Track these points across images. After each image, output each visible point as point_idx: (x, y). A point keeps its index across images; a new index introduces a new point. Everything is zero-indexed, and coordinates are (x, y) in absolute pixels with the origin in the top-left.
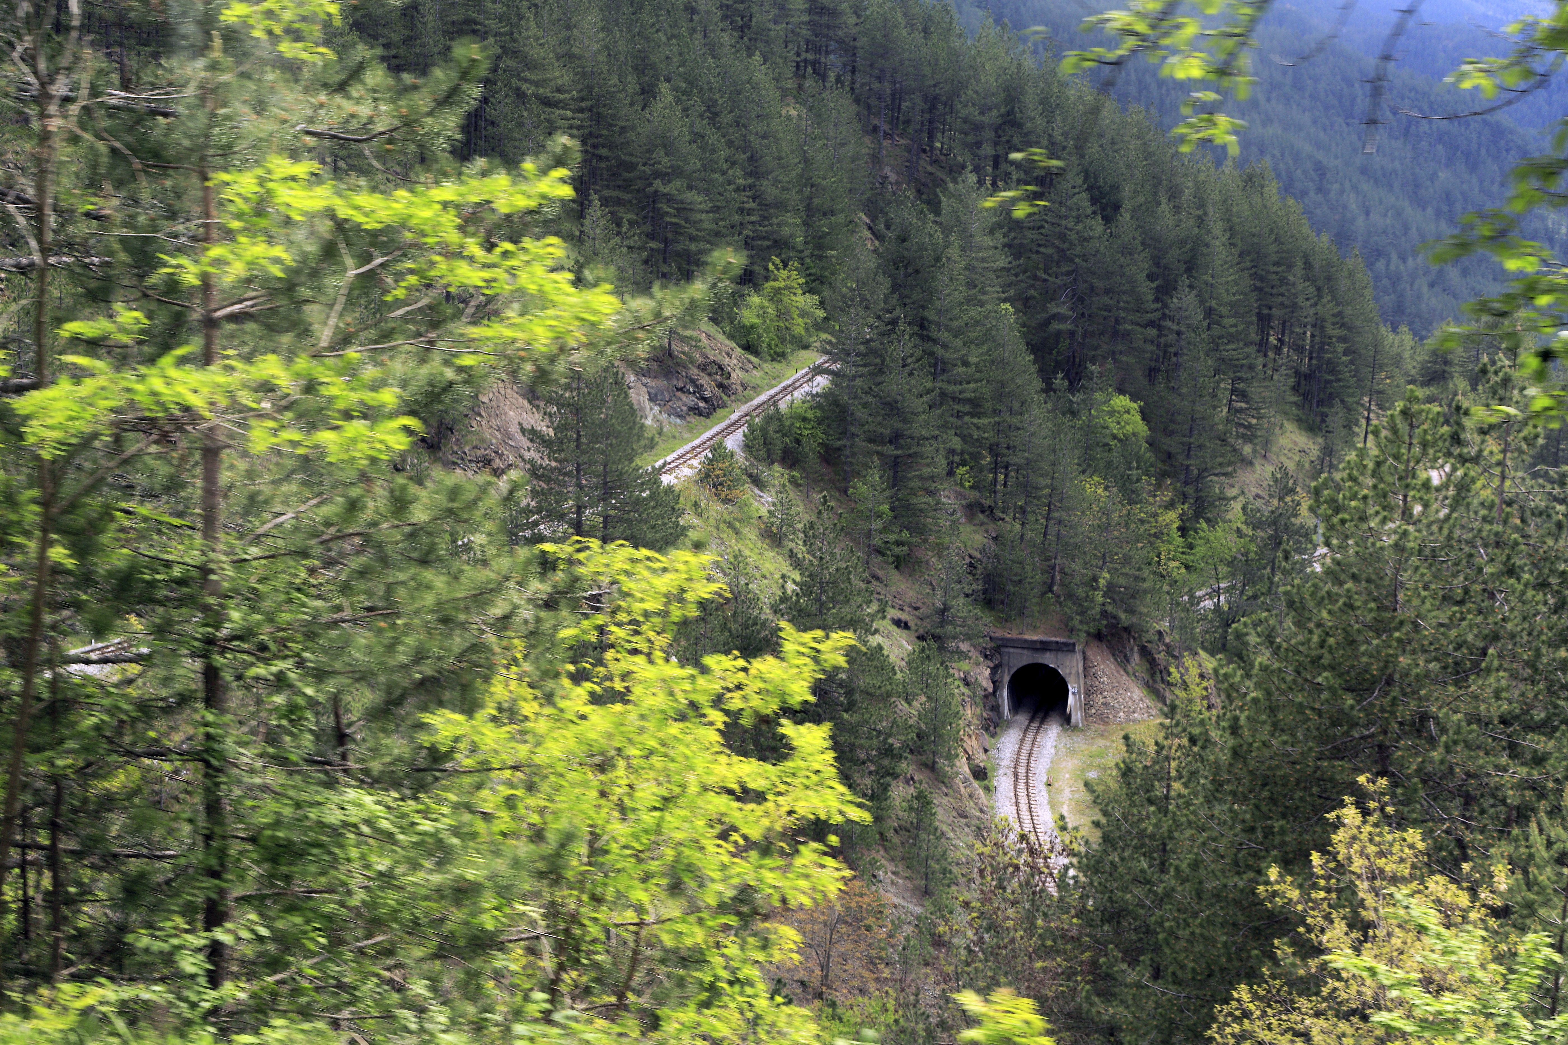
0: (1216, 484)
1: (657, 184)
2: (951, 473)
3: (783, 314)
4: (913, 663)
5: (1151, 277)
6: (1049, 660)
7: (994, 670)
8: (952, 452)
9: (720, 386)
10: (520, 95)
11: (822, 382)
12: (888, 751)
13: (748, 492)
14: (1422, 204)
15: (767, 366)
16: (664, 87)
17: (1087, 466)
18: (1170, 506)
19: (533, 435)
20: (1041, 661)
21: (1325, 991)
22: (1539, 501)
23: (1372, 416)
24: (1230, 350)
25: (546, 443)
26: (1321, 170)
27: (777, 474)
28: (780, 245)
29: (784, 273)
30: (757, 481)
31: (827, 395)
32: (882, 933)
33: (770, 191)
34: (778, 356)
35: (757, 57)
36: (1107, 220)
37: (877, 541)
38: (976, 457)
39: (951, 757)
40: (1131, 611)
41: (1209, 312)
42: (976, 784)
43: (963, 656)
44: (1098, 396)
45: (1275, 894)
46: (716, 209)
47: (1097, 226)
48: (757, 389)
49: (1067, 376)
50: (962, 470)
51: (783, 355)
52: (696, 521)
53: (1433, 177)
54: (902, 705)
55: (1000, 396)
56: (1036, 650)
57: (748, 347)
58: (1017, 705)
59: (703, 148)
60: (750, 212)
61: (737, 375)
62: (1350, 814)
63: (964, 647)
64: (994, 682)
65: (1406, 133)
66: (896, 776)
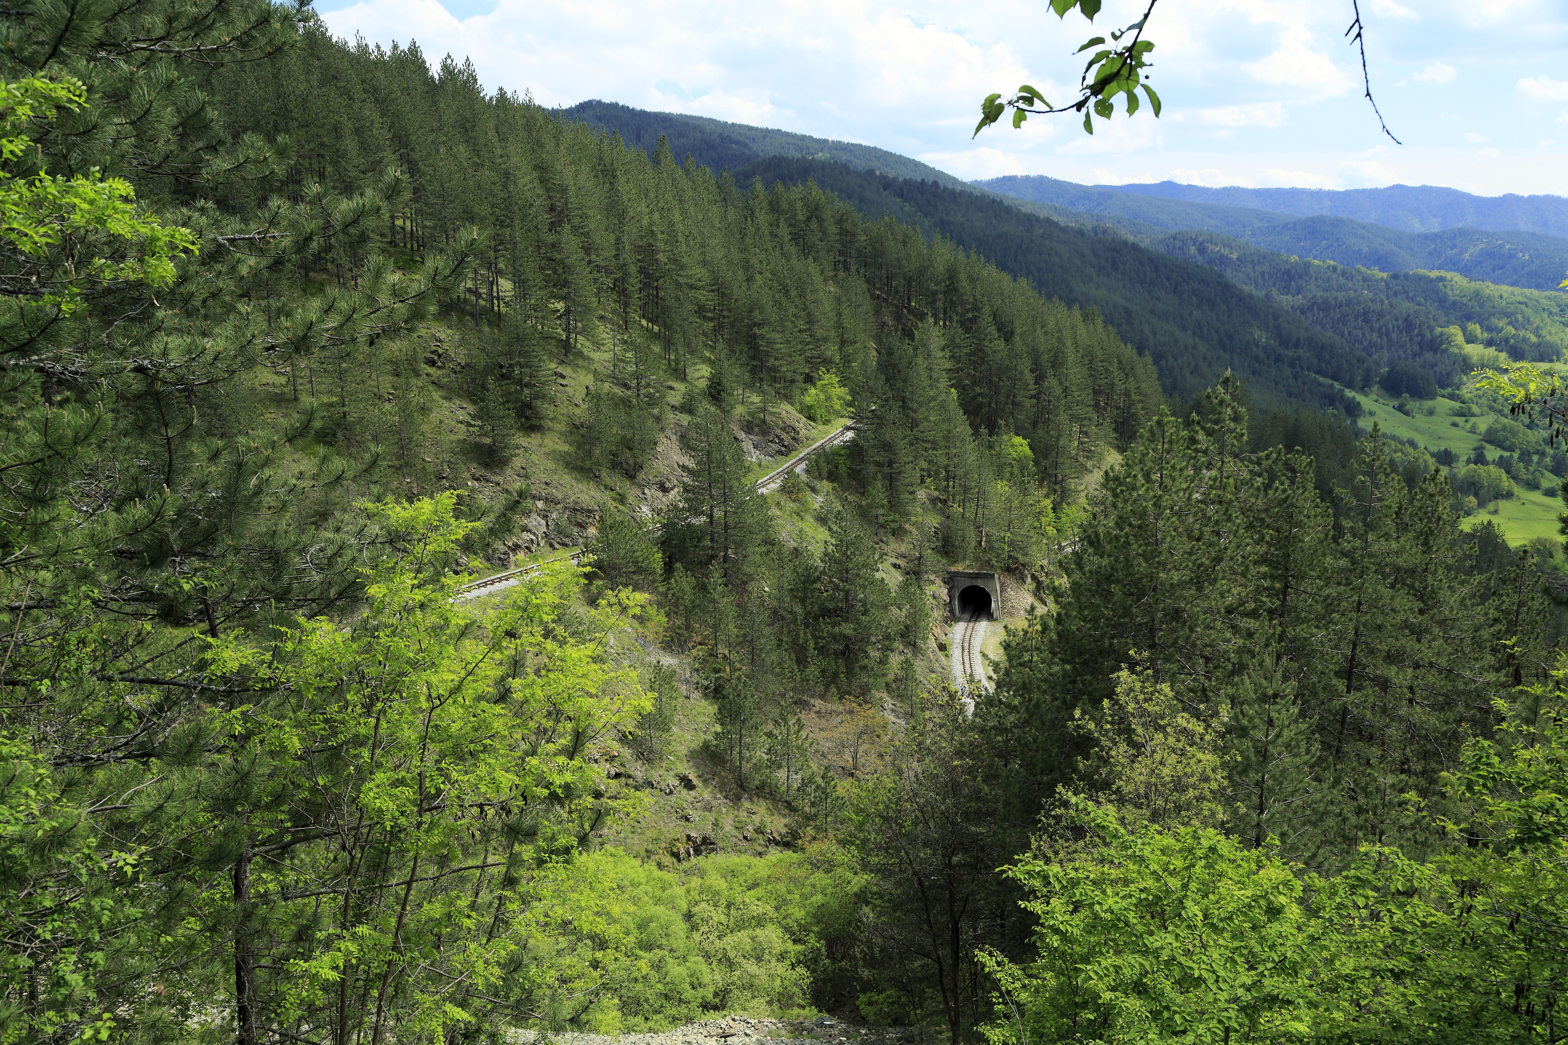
0: (1072, 484)
1: (756, 330)
2: (923, 481)
3: (828, 398)
4: (904, 587)
5: (1032, 371)
6: (980, 583)
7: (950, 590)
8: (922, 470)
9: (794, 439)
10: (678, 284)
11: (850, 435)
12: (888, 637)
13: (809, 496)
14: (1184, 328)
15: (821, 427)
16: (758, 277)
17: (999, 475)
18: (1047, 496)
19: (684, 468)
21: (1114, 787)
22: (1246, 475)
24: (1078, 410)
25: (691, 472)
26: (1128, 312)
27: (826, 485)
28: (827, 362)
29: (827, 376)
30: (814, 490)
31: (853, 441)
32: (886, 739)
33: (819, 333)
34: (827, 422)
35: (810, 259)
36: (1007, 340)
37: (881, 520)
38: (937, 473)
39: (925, 638)
40: (1026, 555)
41: (1066, 389)
42: (940, 653)
43: (933, 582)
44: (1005, 437)
45: (1078, 726)
46: (788, 342)
47: (1002, 344)
48: (814, 440)
49: (987, 427)
50: (929, 480)
51: (829, 421)
52: (778, 513)
53: (1190, 314)
54: (894, 610)
55: (947, 438)
57: (811, 418)
58: (963, 609)
59: (780, 309)
60: (808, 343)
61: (803, 432)
62: (1124, 674)
63: (932, 577)
65: (1175, 291)
66: (892, 651)
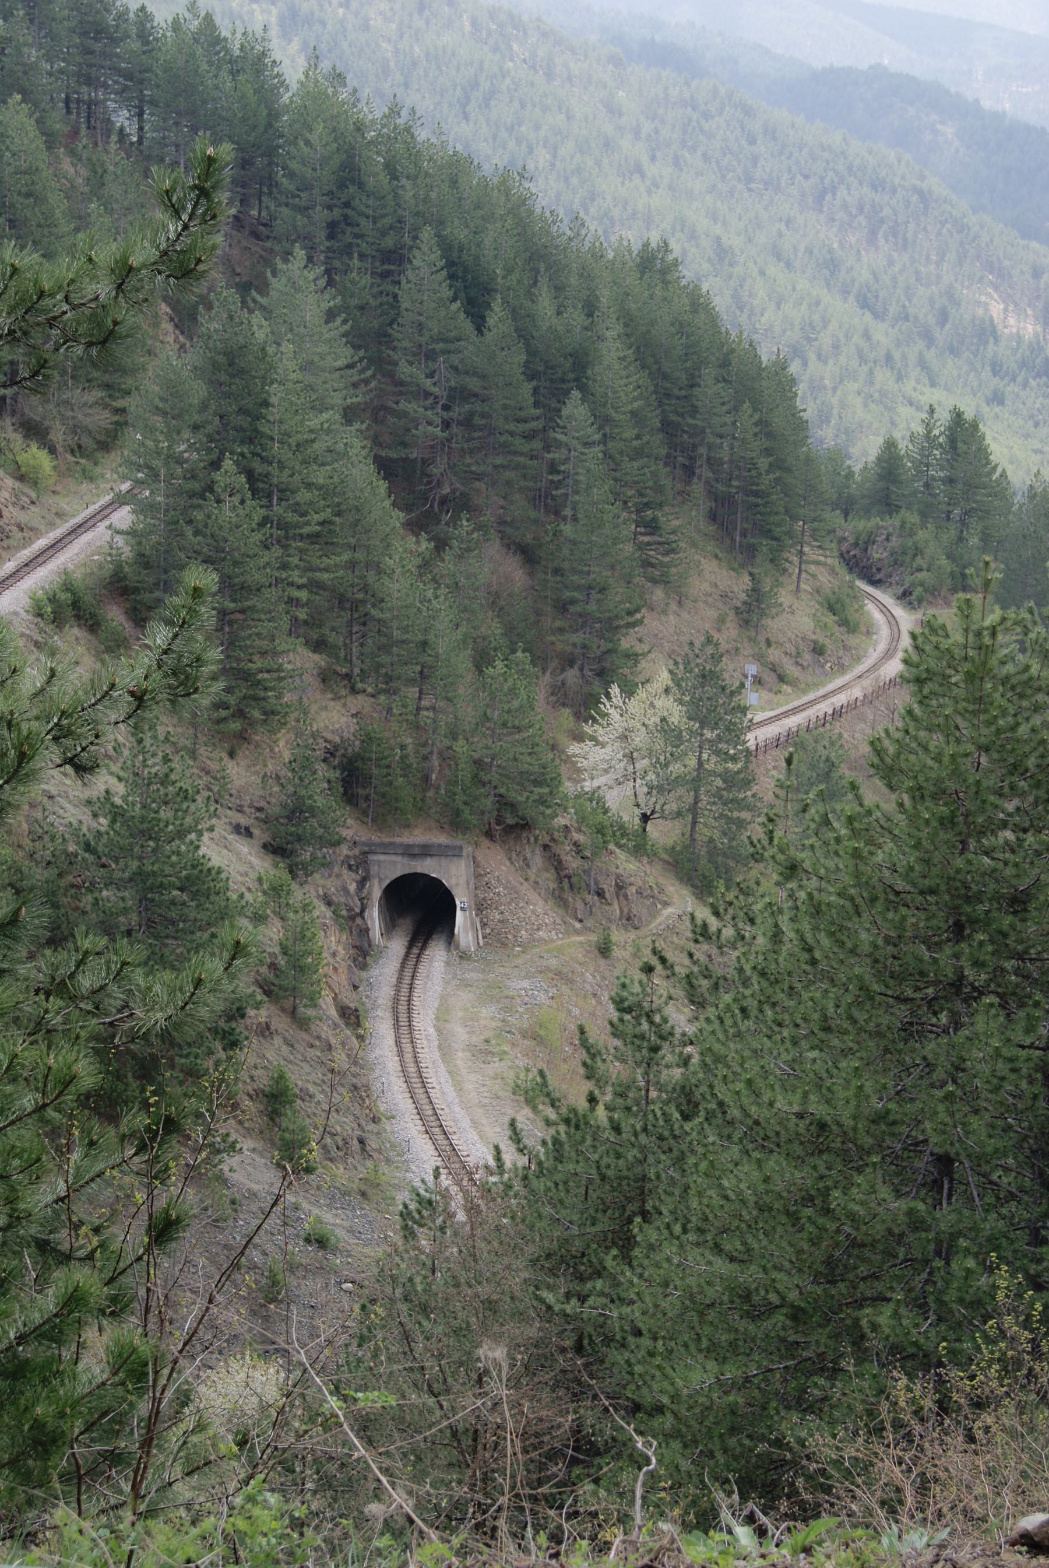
6: (429, 867)
11: (123, 518)
20: (419, 870)
23: (806, 549)
48: (36, 532)
56: (413, 856)
64: (361, 899)
